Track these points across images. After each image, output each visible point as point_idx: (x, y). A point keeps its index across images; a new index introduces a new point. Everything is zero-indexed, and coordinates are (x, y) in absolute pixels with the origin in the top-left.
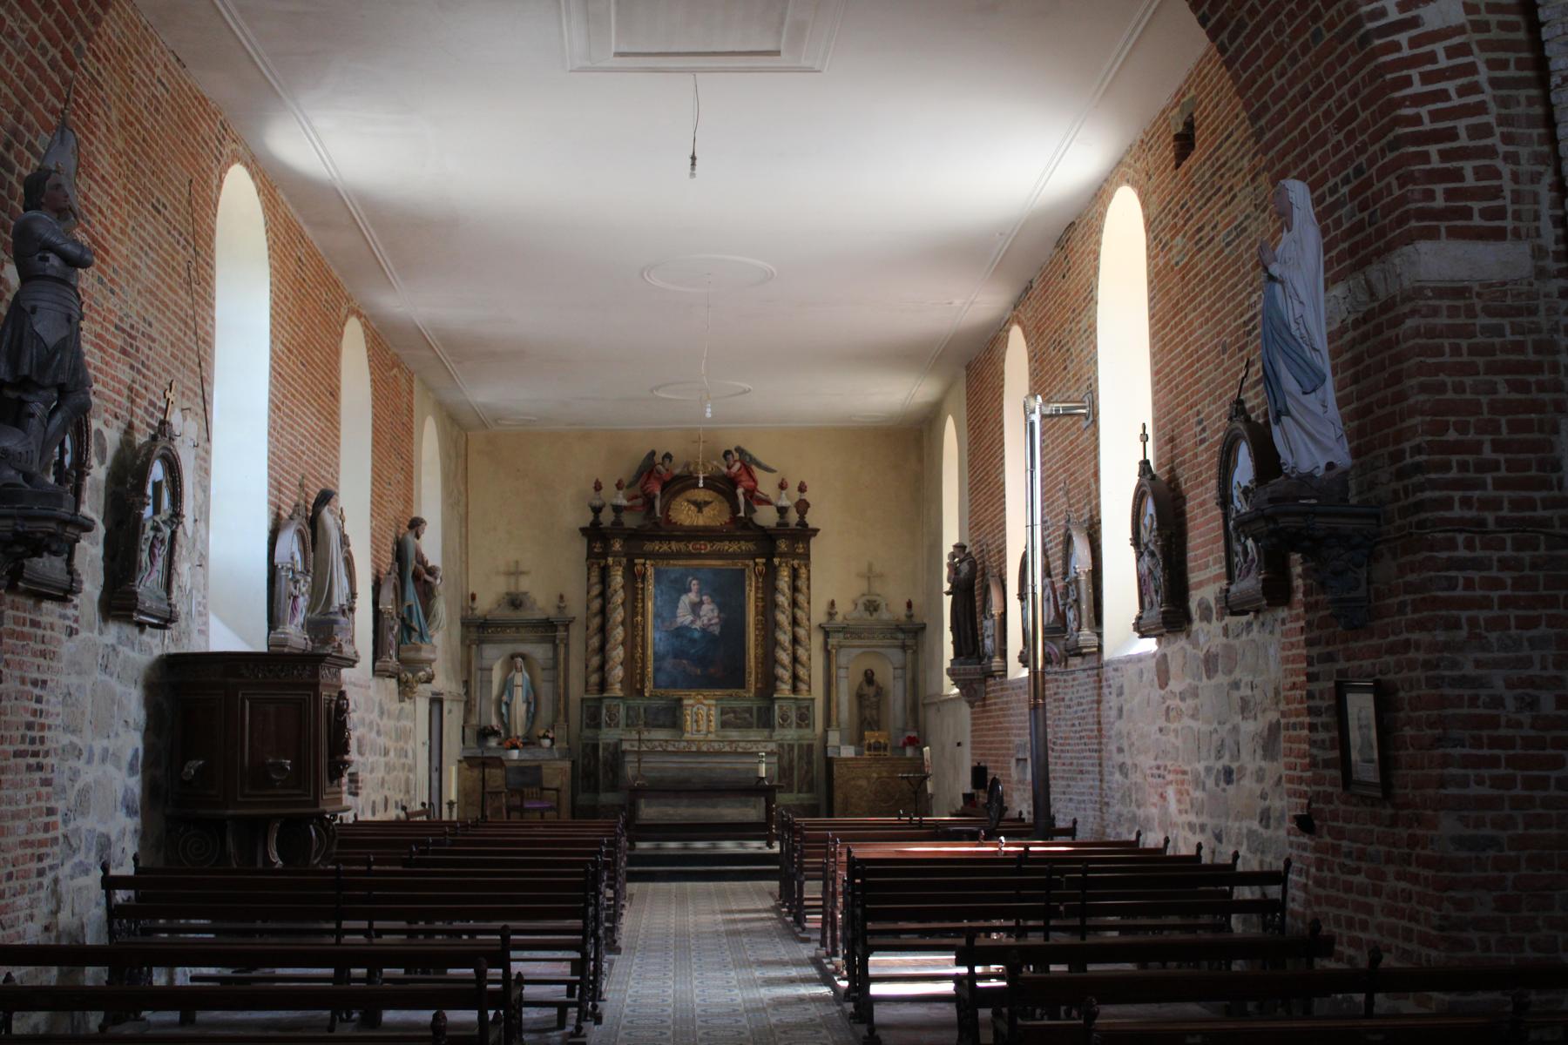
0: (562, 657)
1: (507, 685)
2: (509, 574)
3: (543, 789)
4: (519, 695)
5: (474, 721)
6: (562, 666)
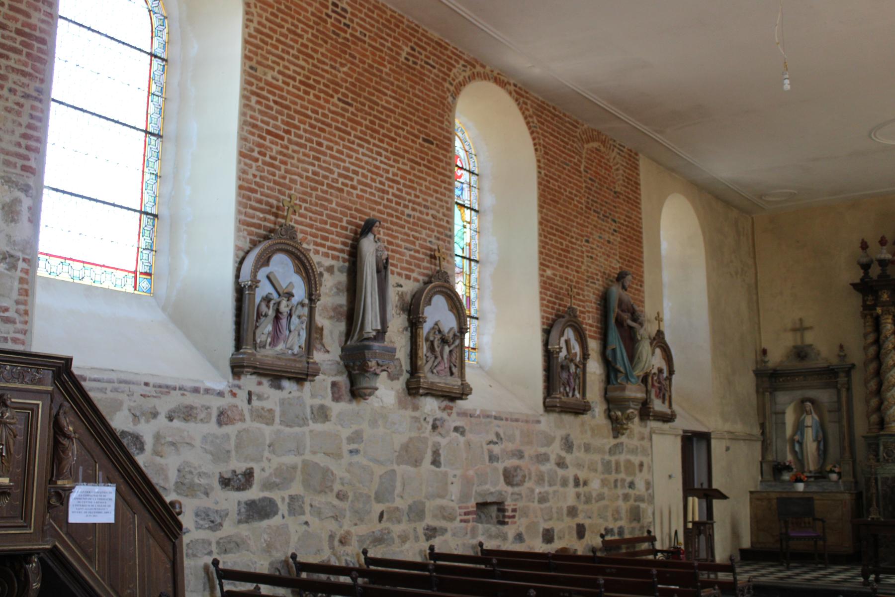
0: (844, 399)
1: (799, 427)
2: (794, 330)
3: (815, 519)
4: (809, 434)
5: (770, 458)
6: (844, 408)
